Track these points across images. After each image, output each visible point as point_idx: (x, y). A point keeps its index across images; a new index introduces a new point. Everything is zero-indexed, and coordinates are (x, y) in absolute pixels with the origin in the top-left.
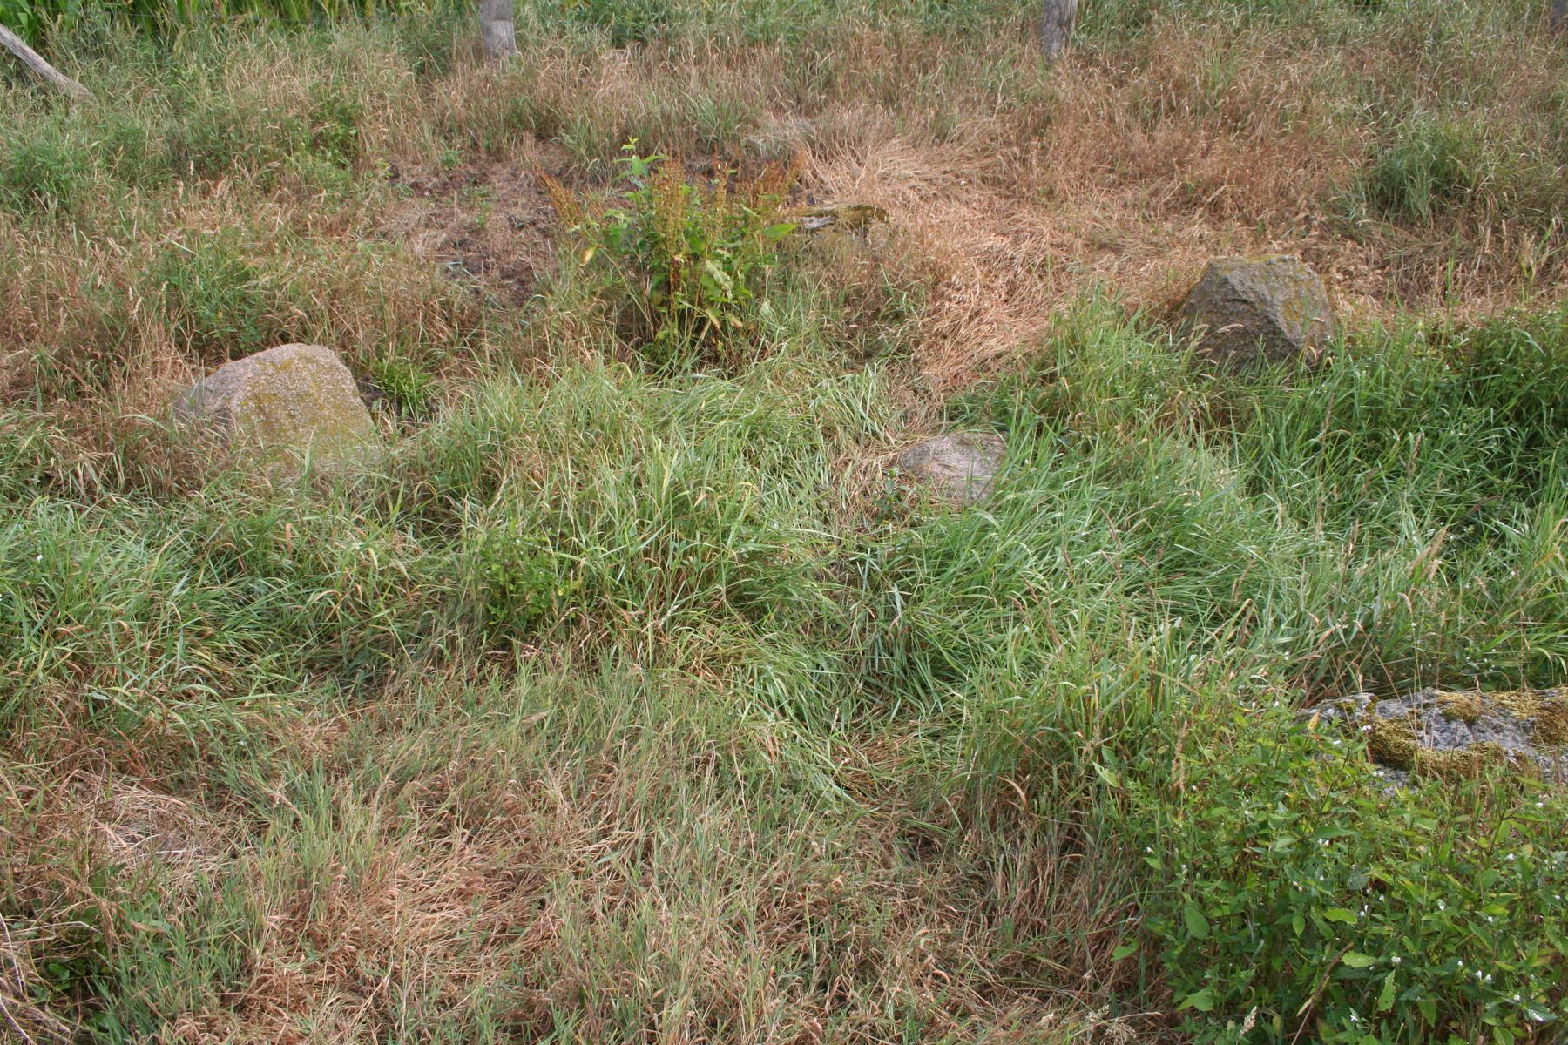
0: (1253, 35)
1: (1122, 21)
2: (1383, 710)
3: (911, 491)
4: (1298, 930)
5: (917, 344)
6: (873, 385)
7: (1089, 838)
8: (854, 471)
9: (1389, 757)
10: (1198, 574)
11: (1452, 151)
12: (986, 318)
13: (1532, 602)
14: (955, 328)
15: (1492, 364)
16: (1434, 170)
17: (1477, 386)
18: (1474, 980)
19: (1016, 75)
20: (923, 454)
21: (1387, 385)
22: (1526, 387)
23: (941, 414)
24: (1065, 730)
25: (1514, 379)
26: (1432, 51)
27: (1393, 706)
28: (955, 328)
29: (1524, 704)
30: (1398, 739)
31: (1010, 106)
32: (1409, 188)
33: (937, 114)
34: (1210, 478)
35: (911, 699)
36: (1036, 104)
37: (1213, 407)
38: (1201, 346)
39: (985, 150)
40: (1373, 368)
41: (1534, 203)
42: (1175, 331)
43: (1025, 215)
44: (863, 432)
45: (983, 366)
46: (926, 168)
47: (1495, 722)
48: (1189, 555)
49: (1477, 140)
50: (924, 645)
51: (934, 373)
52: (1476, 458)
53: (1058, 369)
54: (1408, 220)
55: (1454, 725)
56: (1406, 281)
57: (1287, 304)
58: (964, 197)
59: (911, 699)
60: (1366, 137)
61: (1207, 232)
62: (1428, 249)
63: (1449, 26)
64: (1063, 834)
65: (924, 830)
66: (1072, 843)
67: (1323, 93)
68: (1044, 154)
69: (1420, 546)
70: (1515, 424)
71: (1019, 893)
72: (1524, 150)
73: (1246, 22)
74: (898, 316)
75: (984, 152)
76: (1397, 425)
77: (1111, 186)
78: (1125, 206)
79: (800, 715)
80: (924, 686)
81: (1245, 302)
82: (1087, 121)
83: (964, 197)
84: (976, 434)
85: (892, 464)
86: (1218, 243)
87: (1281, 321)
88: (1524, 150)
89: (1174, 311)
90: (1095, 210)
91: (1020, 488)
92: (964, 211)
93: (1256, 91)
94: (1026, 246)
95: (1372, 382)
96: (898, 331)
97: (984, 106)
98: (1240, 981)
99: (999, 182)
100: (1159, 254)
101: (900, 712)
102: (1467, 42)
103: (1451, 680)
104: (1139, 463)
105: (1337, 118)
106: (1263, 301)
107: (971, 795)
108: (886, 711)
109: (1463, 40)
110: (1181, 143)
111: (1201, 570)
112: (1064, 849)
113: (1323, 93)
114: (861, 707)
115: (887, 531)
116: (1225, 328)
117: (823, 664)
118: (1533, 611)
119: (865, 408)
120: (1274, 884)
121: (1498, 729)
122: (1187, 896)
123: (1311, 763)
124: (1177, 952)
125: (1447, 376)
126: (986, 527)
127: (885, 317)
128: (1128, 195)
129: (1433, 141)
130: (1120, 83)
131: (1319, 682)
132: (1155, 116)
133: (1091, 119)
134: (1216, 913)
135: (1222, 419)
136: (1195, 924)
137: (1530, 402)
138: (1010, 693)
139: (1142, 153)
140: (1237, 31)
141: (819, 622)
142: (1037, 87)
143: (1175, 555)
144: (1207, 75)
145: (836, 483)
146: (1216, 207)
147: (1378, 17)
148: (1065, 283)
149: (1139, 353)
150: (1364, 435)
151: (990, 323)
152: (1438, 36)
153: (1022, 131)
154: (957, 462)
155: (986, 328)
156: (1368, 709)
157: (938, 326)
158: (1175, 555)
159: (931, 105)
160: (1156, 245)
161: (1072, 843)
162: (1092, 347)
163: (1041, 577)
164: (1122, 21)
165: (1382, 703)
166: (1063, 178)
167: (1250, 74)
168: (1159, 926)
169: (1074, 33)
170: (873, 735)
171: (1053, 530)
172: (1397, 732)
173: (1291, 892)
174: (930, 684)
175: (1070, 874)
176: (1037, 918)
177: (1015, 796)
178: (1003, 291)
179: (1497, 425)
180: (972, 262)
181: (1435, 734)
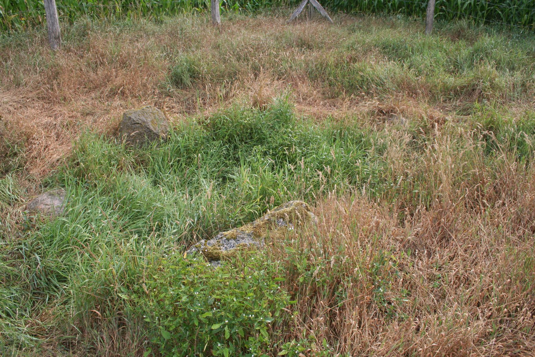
0: (124, 35)
1: (79, 35)
2: (209, 244)
3: (35, 217)
4: (197, 324)
5: (25, 163)
6: (11, 182)
7: (126, 319)
8: (11, 216)
9: (213, 258)
10: (143, 217)
11: (193, 64)
12: (51, 147)
13: (244, 197)
14: (39, 154)
15: (218, 127)
16: (189, 71)
17: (216, 135)
18: (250, 318)
19: (43, 58)
20: (37, 203)
21: (189, 141)
22: (229, 132)
23: (41, 186)
24: (108, 285)
25: (225, 130)
26: (181, 34)
27: (212, 241)
28: (39, 154)
29: (248, 228)
30: (215, 251)
31: (43, 70)
32: (183, 77)
33: (14, 77)
34: (139, 184)
35: (52, 293)
36: (52, 68)
37: (136, 160)
38: (127, 141)
39: (37, 87)
40: (183, 137)
41: (219, 76)
42: (117, 138)
43: (57, 108)
44: (11, 200)
45: (53, 166)
46: (15, 97)
47: (242, 236)
48: (138, 212)
49: (199, 60)
50: (52, 272)
51: (35, 172)
52: (220, 157)
53: (79, 160)
54: (185, 87)
55: (230, 241)
56: (189, 106)
57: (152, 121)
58: (33, 105)
59: (52, 293)
60: (167, 63)
61: (123, 103)
62: (193, 95)
63: (184, 26)
64: (117, 322)
65: (67, 339)
66: (121, 323)
67: (150, 51)
68: (59, 86)
69: (208, 187)
70: (229, 144)
71: (107, 347)
72: (213, 61)
73: (121, 31)
74: (15, 154)
75: (36, 88)
76: (195, 152)
77: (86, 93)
78: (92, 99)
79: (8, 315)
80: (56, 287)
81: (138, 123)
82: (72, 72)
83: (33, 105)
84: (55, 190)
85: (26, 209)
86: (127, 105)
87: (151, 128)
88: (213, 61)
89: (116, 132)
90: (81, 103)
91: (73, 206)
92: (33, 111)
93: (129, 54)
94: (59, 119)
95: (184, 140)
96: (16, 160)
97: (32, 71)
98: (184, 348)
99: (44, 98)
100: (108, 113)
101: (49, 299)
102: (190, 30)
103: (226, 228)
104: (114, 186)
105: (156, 59)
106: (144, 122)
107: (81, 321)
108: (44, 301)
109: (190, 30)
110: (107, 74)
111: (144, 216)
112: (119, 326)
113: (150, 51)
114: (34, 302)
115: (29, 235)
116: (133, 134)
117: (14, 292)
118: (245, 199)
119: (10, 192)
120: (186, 312)
121: (243, 238)
122: (161, 327)
123: (190, 269)
124: (163, 347)
125: (206, 133)
126: (64, 223)
127: (10, 156)
128: (93, 95)
129: (187, 62)
130: (82, 57)
131: (186, 242)
132: (96, 66)
133: (74, 70)
134: (171, 329)
135: (141, 163)
136: (166, 335)
137: (231, 136)
138: (84, 279)
139: (94, 80)
140: (119, 35)
141: (9, 277)
142: (50, 63)
143: (133, 213)
144: (111, 51)
145: (4, 222)
146: (123, 93)
147: (163, 25)
148: (77, 130)
149: (107, 148)
150: (185, 158)
151: (53, 149)
152: (182, 30)
153: (49, 78)
154: (50, 202)
155: (51, 151)
156: (204, 245)
157: (32, 155)
158: (133, 213)
159: (11, 74)
160: (106, 110)
161: (121, 323)
162: (89, 151)
163: (88, 235)
164: (79, 35)
165: (208, 241)
166: (68, 93)
167: (126, 48)
168: (155, 340)
169: (61, 41)
170: (41, 311)
171: (89, 216)
172: (215, 249)
173: (192, 313)
174: (58, 285)
175: (123, 333)
176: (116, 354)
177: (97, 315)
178: (55, 136)
179: (224, 145)
180: (40, 129)
181: (226, 246)
